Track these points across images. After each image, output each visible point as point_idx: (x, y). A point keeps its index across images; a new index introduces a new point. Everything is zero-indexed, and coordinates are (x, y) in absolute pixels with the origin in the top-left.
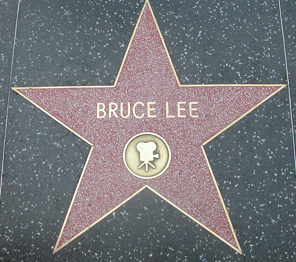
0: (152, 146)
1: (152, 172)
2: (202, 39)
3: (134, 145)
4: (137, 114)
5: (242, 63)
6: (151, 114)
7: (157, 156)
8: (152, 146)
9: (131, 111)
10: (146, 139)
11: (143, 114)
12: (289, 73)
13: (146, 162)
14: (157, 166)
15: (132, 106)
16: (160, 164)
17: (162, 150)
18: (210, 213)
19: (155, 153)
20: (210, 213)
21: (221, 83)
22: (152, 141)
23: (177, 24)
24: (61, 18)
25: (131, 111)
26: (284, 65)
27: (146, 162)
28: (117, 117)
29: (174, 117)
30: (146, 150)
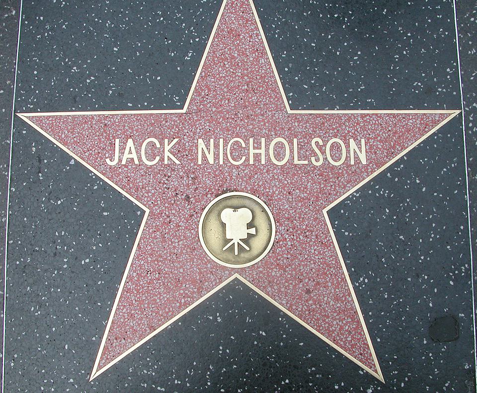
0: (245, 215)
2: (307, 39)
3: (216, 212)
5: (463, 272)
7: (252, 231)
8: (245, 215)
9: (348, 151)
11: (158, 158)
12: (469, 169)
13: (236, 241)
14: (252, 247)
16: (258, 244)
17: (261, 222)
19: (250, 225)
23: (392, 193)
24: (262, 10)
25: (348, 151)
27: (236, 241)
29: (306, 162)
30: (236, 223)
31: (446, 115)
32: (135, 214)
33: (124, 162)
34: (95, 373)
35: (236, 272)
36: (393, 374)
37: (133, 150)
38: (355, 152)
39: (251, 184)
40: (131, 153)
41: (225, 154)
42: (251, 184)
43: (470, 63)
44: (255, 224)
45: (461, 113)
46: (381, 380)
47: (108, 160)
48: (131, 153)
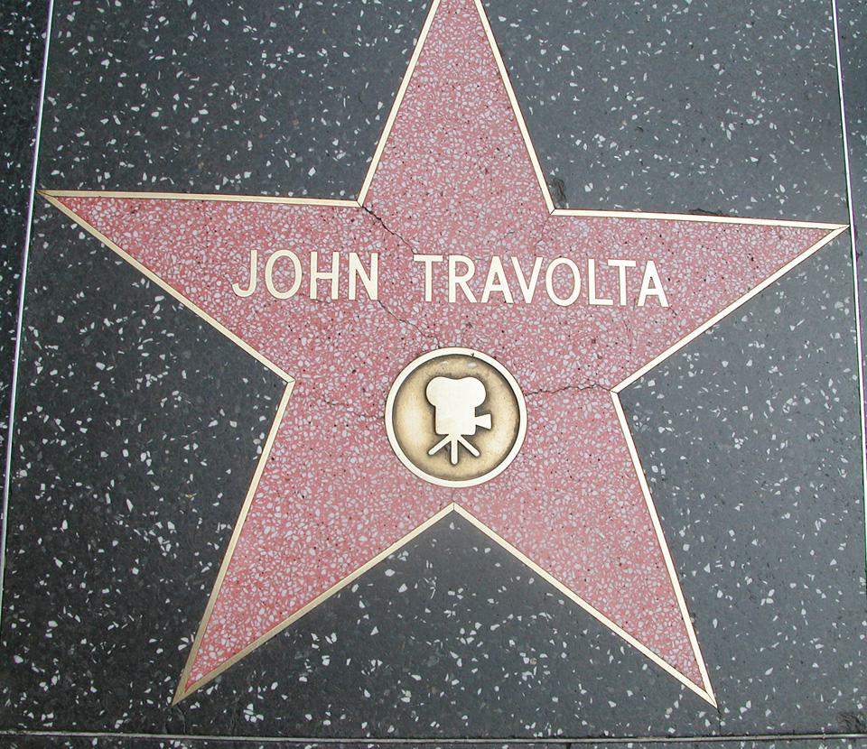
0: (473, 392)
1: (470, 466)
3: (422, 384)
4: (276, 281)
6: (471, 283)
8: (473, 392)
9: (261, 274)
10: (458, 366)
13: (454, 438)
15: (545, 265)
16: (495, 444)
18: (267, 575)
19: (479, 411)
20: (267, 575)
21: (381, 128)
22: (469, 376)
25: (261, 274)
26: (841, 10)
27: (454, 438)
28: (472, 299)
30: (457, 401)
31: (528, 274)
32: (277, 386)
33: (485, 299)
34: (709, 696)
35: (457, 497)
36: (743, 715)
37: (657, 282)
38: (368, 273)
39: (490, 338)
40: (654, 287)
41: (584, 275)
42: (490, 338)
43: (4, 433)
44: (492, 410)
45: (850, 228)
46: (712, 703)
47: (236, 287)
48: (654, 287)
